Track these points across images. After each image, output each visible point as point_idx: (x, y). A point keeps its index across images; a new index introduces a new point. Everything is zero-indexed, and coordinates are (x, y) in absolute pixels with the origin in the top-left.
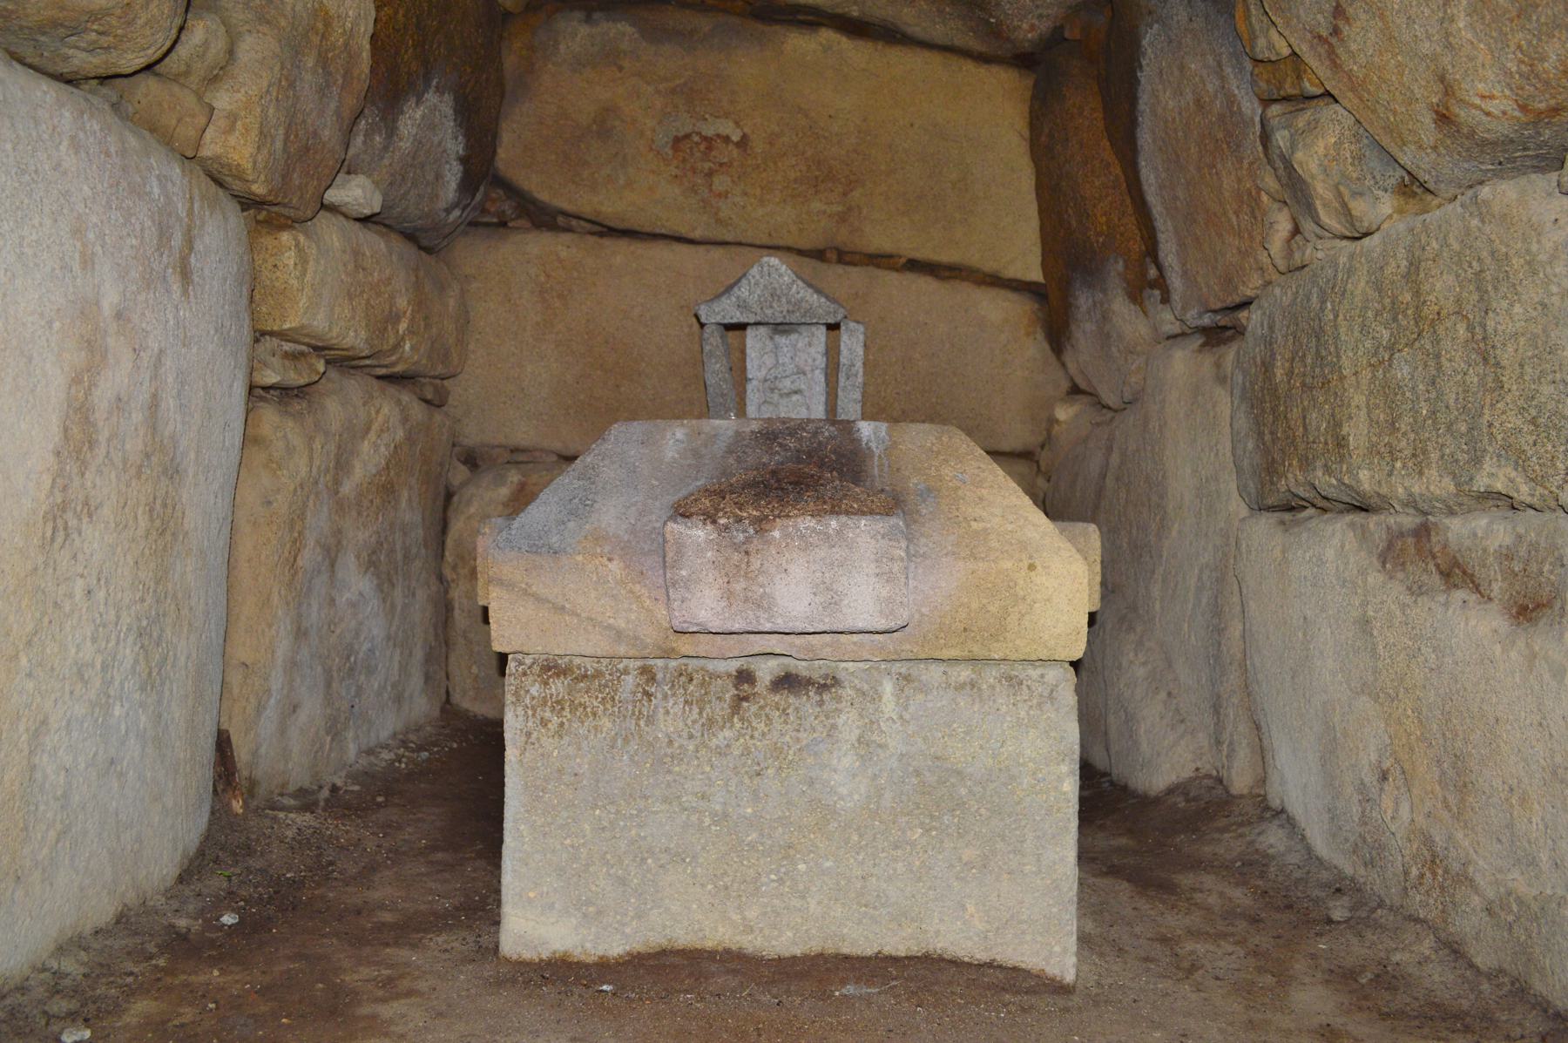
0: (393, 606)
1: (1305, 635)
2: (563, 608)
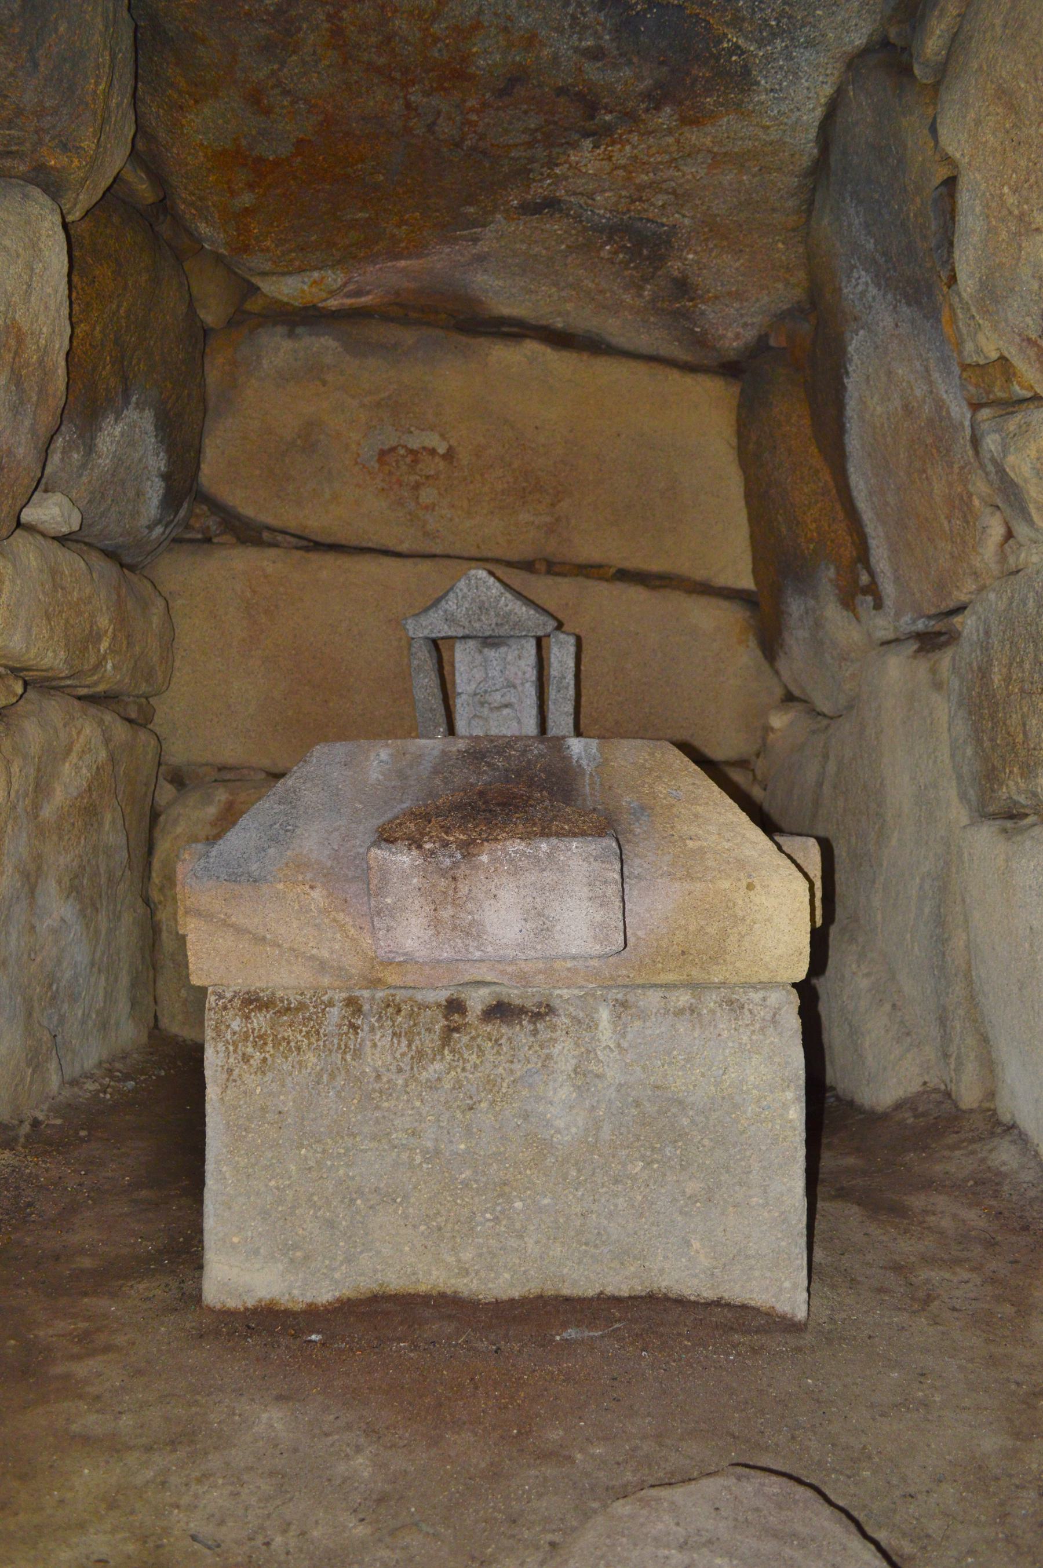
0: (97, 931)
1: (1031, 946)
2: (264, 938)
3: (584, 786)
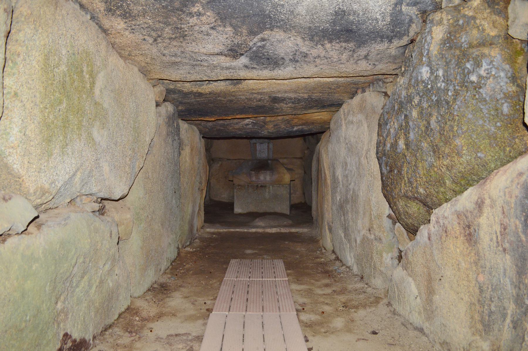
3: (315, 82)
